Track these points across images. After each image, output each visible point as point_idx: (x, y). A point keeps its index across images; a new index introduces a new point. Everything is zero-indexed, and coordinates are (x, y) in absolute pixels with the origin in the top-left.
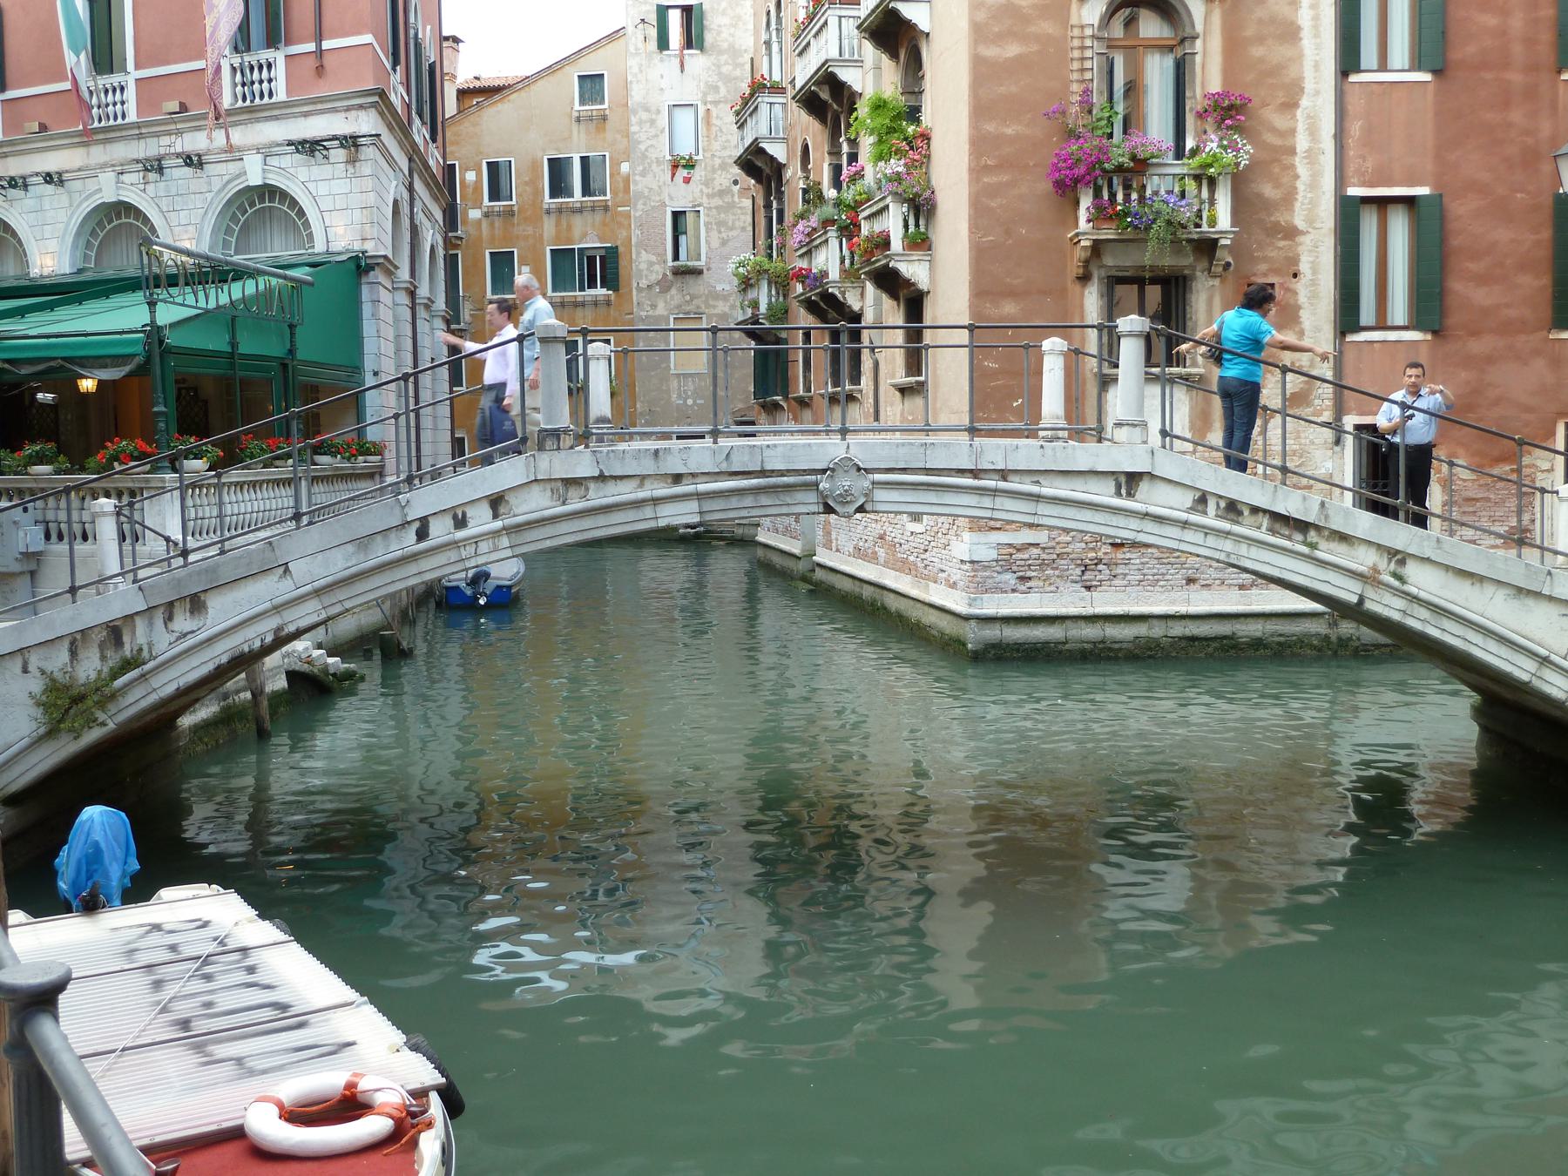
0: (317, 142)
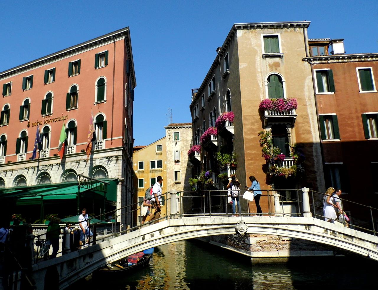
0: (111, 157)
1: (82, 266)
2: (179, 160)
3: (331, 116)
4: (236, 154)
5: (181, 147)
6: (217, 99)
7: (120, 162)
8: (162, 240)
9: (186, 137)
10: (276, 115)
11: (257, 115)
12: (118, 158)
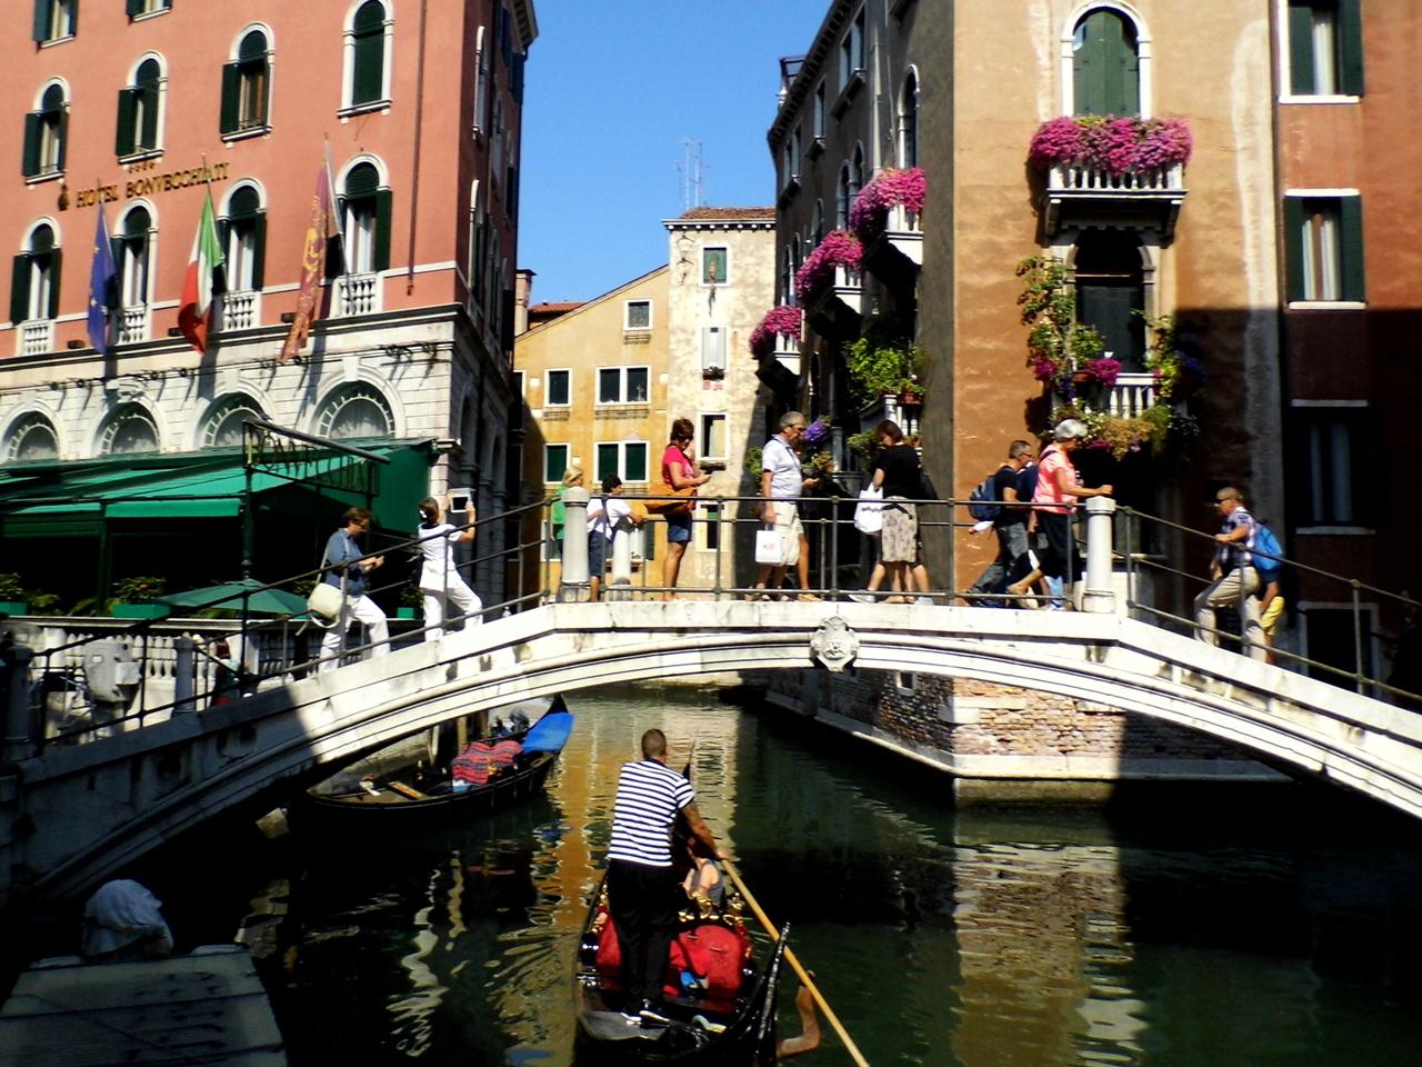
0: (404, 348)
1: (214, 769)
2: (722, 370)
3: (1337, 200)
4: (923, 353)
5: (735, 310)
6: (869, 109)
7: (444, 372)
8: (524, 683)
9: (757, 268)
10: (1098, 186)
11: (1019, 187)
12: (435, 355)
